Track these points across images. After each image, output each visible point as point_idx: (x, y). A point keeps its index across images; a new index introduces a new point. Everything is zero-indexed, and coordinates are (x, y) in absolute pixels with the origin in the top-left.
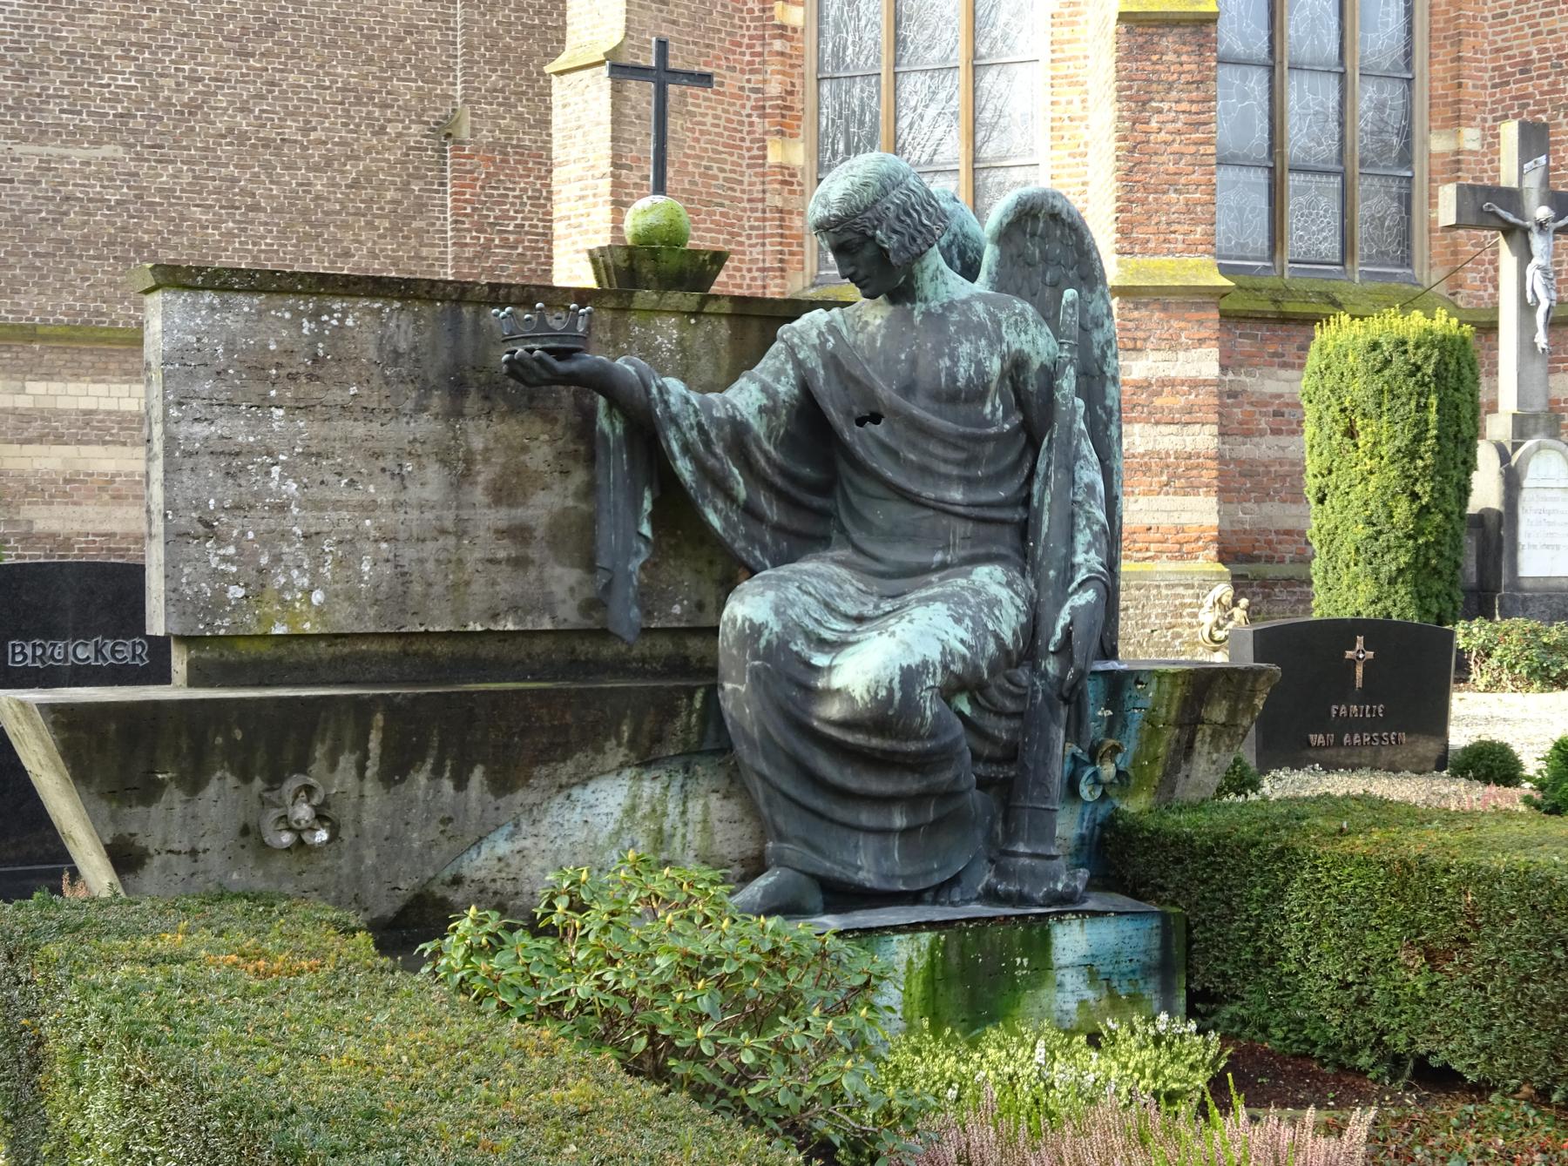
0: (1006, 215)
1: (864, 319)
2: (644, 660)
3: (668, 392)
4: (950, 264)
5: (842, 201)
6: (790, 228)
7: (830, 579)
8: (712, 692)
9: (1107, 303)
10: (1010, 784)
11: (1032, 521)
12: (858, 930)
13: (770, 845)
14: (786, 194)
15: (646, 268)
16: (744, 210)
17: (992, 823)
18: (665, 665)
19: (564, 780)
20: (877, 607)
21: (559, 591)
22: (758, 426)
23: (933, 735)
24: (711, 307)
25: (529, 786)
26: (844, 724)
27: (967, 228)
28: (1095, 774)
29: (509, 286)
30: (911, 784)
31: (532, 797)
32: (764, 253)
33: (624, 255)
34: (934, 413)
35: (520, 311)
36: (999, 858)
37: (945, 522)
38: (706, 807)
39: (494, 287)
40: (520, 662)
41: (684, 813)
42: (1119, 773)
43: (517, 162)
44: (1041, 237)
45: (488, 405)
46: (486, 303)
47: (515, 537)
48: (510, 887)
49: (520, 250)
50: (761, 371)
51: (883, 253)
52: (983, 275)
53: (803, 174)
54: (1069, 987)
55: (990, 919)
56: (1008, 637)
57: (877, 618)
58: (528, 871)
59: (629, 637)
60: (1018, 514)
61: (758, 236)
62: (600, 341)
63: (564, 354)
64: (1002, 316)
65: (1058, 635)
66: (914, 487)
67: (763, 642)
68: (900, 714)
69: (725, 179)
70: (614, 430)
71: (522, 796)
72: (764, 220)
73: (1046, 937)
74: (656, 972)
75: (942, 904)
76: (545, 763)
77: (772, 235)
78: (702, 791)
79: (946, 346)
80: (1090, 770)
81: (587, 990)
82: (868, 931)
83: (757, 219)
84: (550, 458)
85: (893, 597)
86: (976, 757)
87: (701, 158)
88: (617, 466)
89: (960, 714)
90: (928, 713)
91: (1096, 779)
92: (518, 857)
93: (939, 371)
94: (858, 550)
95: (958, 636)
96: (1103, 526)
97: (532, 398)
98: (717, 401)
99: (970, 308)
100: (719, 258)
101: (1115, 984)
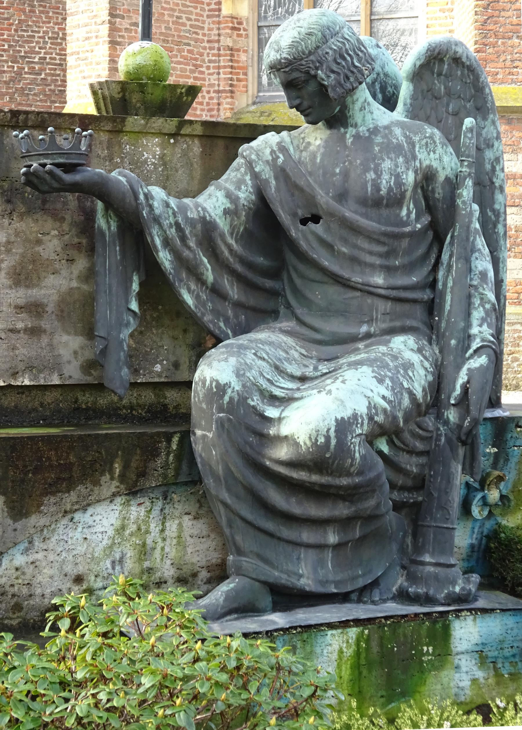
0: (419, 59)
1: (307, 140)
2: (132, 408)
3: (153, 198)
4: (374, 96)
5: (291, 46)
6: (238, 62)
7: (279, 346)
8: (186, 436)
9: (496, 128)
10: (418, 508)
11: (437, 300)
12: (301, 627)
13: (231, 558)
14: (235, 37)
15: (135, 98)
16: (205, 48)
17: (404, 537)
18: (149, 411)
19: (68, 507)
20: (316, 369)
21: (65, 353)
22: (223, 224)
23: (360, 473)
24: (186, 130)
25: (40, 512)
26: (290, 464)
27: (387, 69)
28: (484, 498)
29: (27, 113)
30: (343, 510)
31: (43, 521)
32: (219, 79)
33: (118, 88)
34: (362, 215)
35: (35, 133)
36: (410, 566)
37: (369, 301)
38: (180, 525)
39: (15, 114)
40: (35, 410)
41: (163, 531)
42: (502, 497)
43: (41, 12)
44: (446, 76)
45: (9, 207)
46: (8, 126)
47: (30, 312)
48: (25, 591)
49: (43, 76)
50: (226, 181)
51: (322, 89)
52: (400, 107)
53: (247, 23)
54: (464, 669)
55: (403, 616)
56: (419, 393)
57: (316, 378)
58: (40, 578)
59: (121, 391)
60: (426, 295)
61: (214, 68)
62: (98, 156)
63: (70, 168)
64: (416, 139)
65: (458, 390)
66: (345, 273)
67: (226, 399)
68: (334, 457)
69: (191, 26)
70: (109, 228)
71: (35, 520)
72: (219, 55)
73: (446, 634)
74: (141, 690)
75: (365, 603)
76: (53, 494)
77: (225, 67)
78: (177, 513)
79: (371, 162)
80: (479, 495)
81: (85, 708)
82: (308, 628)
83: (214, 55)
84: (59, 249)
85: (328, 360)
86: (393, 486)
87: (174, 10)
88: (112, 255)
89: (380, 453)
90: (357, 455)
91: (485, 502)
92: (32, 567)
93: (366, 182)
94: (301, 322)
95: (380, 393)
96: (493, 305)
97: (44, 202)
98: (191, 205)
99: (391, 132)
100: (193, 91)
101: (500, 665)
